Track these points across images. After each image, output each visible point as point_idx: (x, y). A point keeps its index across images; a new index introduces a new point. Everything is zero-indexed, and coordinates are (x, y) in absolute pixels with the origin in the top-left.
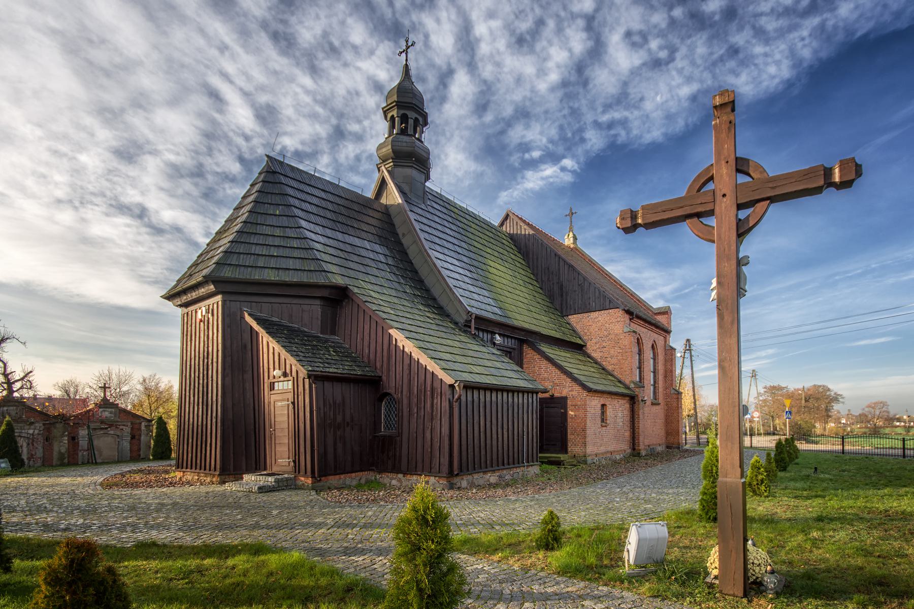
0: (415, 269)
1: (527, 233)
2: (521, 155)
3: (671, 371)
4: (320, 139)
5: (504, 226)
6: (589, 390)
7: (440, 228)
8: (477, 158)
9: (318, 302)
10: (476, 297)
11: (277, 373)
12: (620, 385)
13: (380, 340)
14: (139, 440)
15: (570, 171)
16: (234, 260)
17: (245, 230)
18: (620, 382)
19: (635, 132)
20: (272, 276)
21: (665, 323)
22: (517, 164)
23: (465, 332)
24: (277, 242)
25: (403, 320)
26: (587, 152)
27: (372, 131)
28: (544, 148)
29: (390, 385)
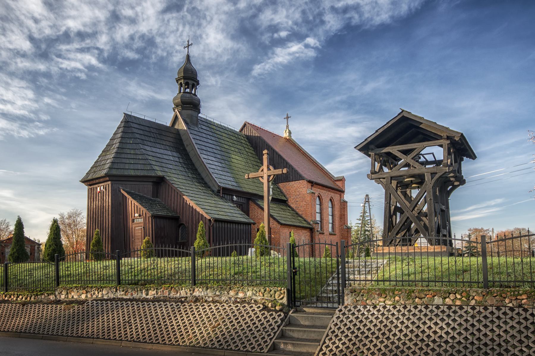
0: (196, 168)
1: (256, 135)
2: (271, 34)
3: (344, 215)
4: (99, 22)
5: (243, 131)
6: (282, 224)
7: (205, 140)
8: (233, 38)
9: (151, 184)
10: (223, 177)
11: (137, 215)
12: (304, 222)
13: (179, 201)
14: (34, 255)
15: (313, 48)
16: (116, 166)
17: (119, 152)
18: (305, 221)
19: (367, 15)
20: (132, 173)
21: (341, 186)
22: (267, 43)
23: (217, 195)
24: (132, 157)
25: (189, 191)
26: (327, 32)
27: (144, 15)
28: (290, 29)
29: (184, 220)
